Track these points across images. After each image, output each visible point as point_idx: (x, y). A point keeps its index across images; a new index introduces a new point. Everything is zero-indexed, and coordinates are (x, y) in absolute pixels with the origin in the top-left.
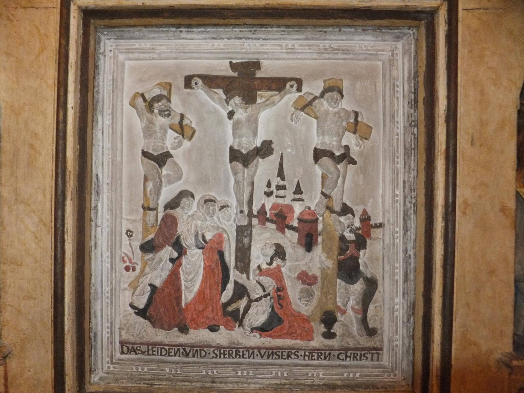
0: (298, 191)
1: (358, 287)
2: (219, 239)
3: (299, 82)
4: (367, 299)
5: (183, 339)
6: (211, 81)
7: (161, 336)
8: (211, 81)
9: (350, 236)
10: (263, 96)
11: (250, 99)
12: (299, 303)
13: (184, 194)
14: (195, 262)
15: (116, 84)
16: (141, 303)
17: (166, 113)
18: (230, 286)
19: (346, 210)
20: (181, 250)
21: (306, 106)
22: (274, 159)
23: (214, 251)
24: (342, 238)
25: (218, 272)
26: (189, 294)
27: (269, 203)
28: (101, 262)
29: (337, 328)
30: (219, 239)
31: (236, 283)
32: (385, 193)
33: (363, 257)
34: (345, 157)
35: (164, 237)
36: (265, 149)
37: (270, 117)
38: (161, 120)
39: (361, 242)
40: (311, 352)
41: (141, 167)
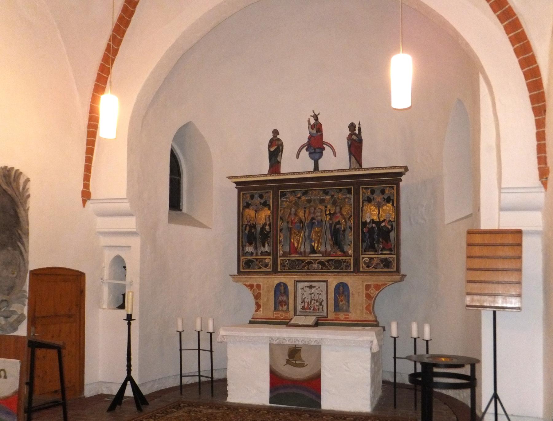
6: (308, 287)
8: (308, 287)
14: (306, 303)
21: (317, 289)
23: (308, 303)
28: (298, 304)
32: (324, 298)
35: (303, 301)
37: (313, 290)
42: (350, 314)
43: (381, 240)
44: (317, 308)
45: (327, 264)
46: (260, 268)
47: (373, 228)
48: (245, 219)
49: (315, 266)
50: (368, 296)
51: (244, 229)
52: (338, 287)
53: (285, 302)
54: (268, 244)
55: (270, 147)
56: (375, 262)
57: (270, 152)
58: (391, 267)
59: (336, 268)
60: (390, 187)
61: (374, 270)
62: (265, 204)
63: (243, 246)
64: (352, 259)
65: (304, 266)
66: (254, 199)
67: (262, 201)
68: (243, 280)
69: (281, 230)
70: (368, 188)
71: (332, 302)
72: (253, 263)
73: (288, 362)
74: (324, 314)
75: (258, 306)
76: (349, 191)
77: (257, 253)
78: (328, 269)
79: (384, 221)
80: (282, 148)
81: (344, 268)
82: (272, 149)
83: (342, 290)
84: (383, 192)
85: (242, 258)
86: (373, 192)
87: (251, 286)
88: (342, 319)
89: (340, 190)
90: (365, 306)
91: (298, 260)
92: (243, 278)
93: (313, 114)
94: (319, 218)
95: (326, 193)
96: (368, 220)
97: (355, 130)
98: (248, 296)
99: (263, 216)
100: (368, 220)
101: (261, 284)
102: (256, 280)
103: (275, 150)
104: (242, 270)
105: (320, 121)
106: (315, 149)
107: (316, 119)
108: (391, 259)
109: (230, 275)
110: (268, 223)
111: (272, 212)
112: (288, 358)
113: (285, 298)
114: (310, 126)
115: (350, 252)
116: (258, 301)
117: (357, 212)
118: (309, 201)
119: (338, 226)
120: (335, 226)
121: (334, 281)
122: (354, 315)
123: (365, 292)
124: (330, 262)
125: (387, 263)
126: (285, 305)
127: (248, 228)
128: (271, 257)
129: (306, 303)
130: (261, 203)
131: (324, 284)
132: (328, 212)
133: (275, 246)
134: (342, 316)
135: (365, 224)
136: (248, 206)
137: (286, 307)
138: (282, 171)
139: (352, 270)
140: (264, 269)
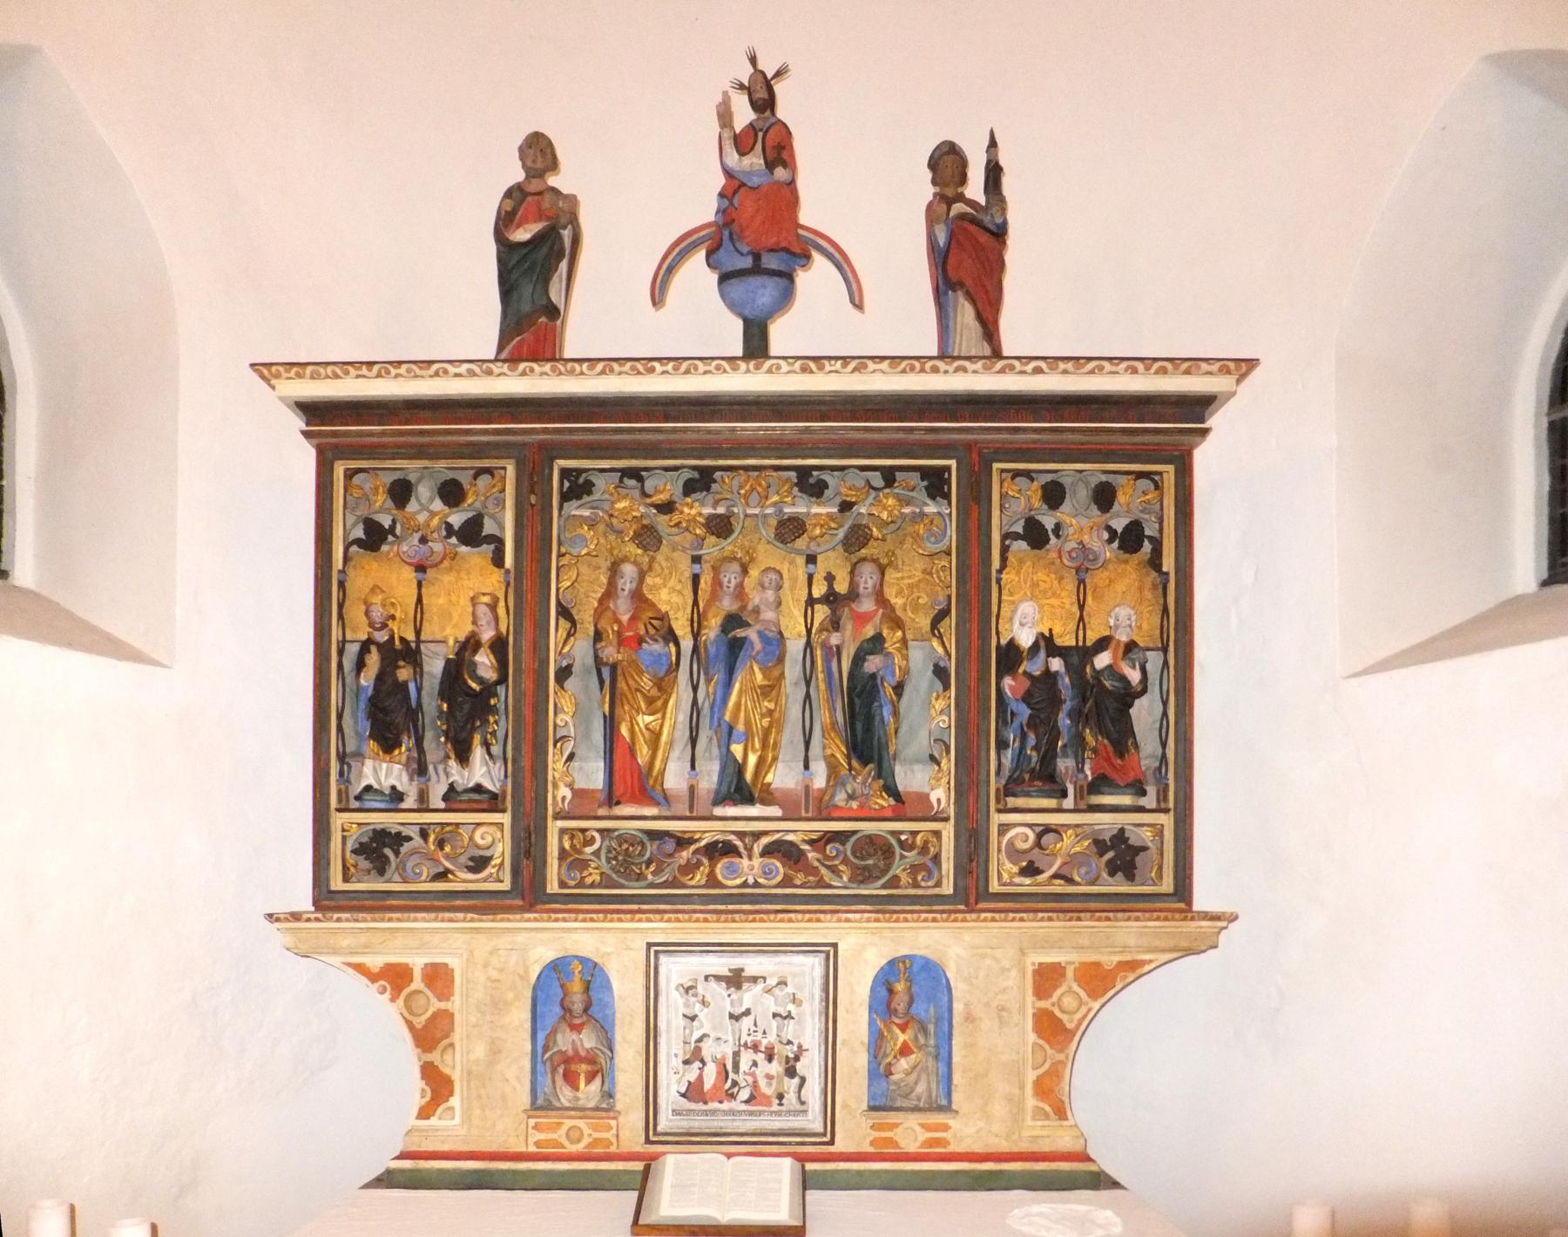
1: (796, 1081)
2: (724, 1058)
3: (765, 979)
4: (801, 1086)
7: (693, 1106)
8: (718, 978)
10: (745, 986)
11: (739, 987)
12: (767, 1089)
13: (705, 1036)
15: (668, 980)
16: (683, 1090)
17: (695, 995)
19: (789, 1042)
20: (703, 1062)
21: (768, 991)
22: (751, 1018)
25: (723, 1073)
26: (708, 1085)
27: (749, 1039)
30: (724, 1058)
32: (808, 1033)
33: (799, 1066)
34: (789, 1016)
35: (695, 1056)
36: (747, 1013)
37: (749, 996)
39: (797, 1059)
41: (682, 1022)
43: (1089, 738)
45: (812, 855)
46: (442, 875)
47: (1049, 676)
48: (355, 613)
49: (750, 867)
50: (1053, 1030)
51: (348, 664)
52: (886, 981)
53: (591, 1059)
54: (487, 745)
55: (505, 221)
56: (1068, 844)
57: (506, 249)
58: (1145, 879)
59: (863, 876)
60: (1140, 475)
61: (1059, 887)
62: (471, 533)
63: (342, 757)
64: (948, 831)
65: (689, 868)
66: (412, 506)
67: (457, 519)
68: (345, 942)
69: (564, 673)
70: (1028, 474)
72: (406, 847)
75: (438, 1086)
76: (936, 484)
77: (423, 796)
78: (822, 884)
79: (1103, 644)
80: (576, 240)
81: (905, 879)
82: (522, 235)
83: (909, 996)
84: (1104, 497)
85: (338, 820)
86: (1054, 495)
87: (395, 978)
88: (912, 1147)
89: (889, 475)
90: (1031, 1076)
91: (653, 835)
92: (348, 930)
93: (745, 73)
94: (768, 615)
95: (810, 485)
96: (1026, 639)
97: (963, 179)
98: (381, 1022)
99: (460, 603)
100: (1026, 639)
101: (454, 962)
102: (421, 941)
103: (535, 254)
104: (337, 883)
105: (783, 112)
106: (757, 257)
107: (764, 101)
108: (1147, 835)
109: (270, 917)
110: (487, 635)
111: (516, 581)
113: (588, 1040)
114: (727, 134)
115: (941, 796)
116: (434, 1057)
117: (975, 598)
118: (721, 527)
119: (872, 664)
120: (858, 660)
121: (867, 945)
122: (971, 1129)
123: (1031, 1004)
124: (830, 849)
125: (1122, 855)
126: (590, 1078)
127: (373, 659)
128: (505, 819)
130: (449, 527)
131: (812, 966)
132: (819, 590)
133: (526, 763)
134: (910, 1132)
135: (1010, 656)
136: (374, 537)
137: (596, 1085)
138: (573, 345)
139: (948, 888)
140: (465, 880)
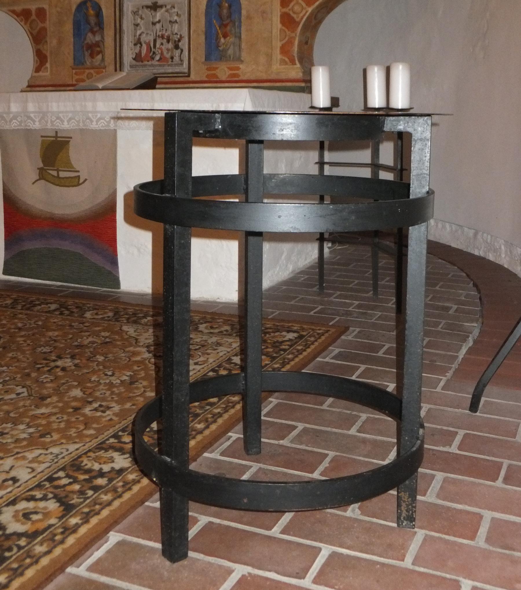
0: (166, 30)
1: (179, 51)
2: (149, 42)
3: (166, 6)
5: (142, 64)
7: (138, 64)
8: (147, 7)
9: (177, 40)
11: (155, 10)
13: (143, 33)
14: (144, 46)
16: (134, 57)
17: (138, 15)
18: (152, 52)
20: (141, 45)
22: (161, 23)
23: (148, 45)
24: (175, 40)
26: (143, 54)
29: (174, 60)
30: (149, 42)
31: (457, 433)
33: (180, 44)
35: (138, 42)
36: (159, 22)
38: (137, 16)
39: (179, 41)
40: (169, 65)
42: (241, 66)
44: (168, 56)
71: (199, 40)
73: (42, 175)
74: (184, 68)
75: (41, 58)
88: (224, 78)
101: (46, 7)
112: (41, 165)
116: (40, 47)
129: (144, 46)
